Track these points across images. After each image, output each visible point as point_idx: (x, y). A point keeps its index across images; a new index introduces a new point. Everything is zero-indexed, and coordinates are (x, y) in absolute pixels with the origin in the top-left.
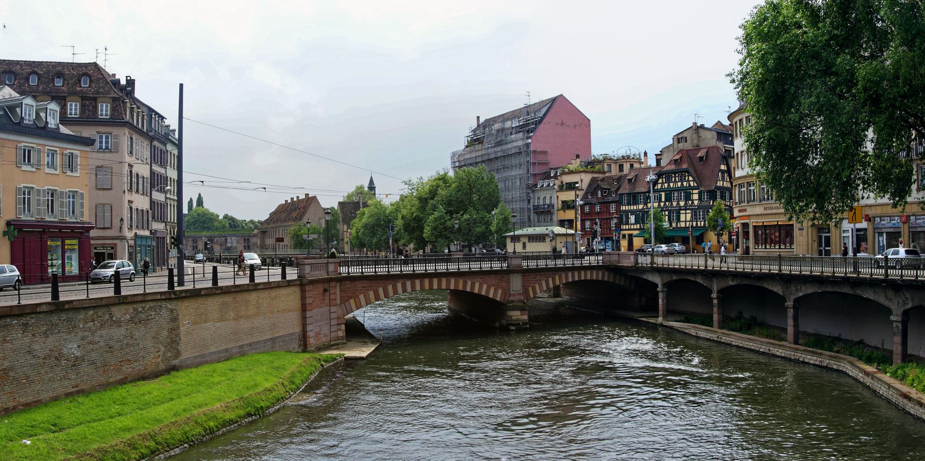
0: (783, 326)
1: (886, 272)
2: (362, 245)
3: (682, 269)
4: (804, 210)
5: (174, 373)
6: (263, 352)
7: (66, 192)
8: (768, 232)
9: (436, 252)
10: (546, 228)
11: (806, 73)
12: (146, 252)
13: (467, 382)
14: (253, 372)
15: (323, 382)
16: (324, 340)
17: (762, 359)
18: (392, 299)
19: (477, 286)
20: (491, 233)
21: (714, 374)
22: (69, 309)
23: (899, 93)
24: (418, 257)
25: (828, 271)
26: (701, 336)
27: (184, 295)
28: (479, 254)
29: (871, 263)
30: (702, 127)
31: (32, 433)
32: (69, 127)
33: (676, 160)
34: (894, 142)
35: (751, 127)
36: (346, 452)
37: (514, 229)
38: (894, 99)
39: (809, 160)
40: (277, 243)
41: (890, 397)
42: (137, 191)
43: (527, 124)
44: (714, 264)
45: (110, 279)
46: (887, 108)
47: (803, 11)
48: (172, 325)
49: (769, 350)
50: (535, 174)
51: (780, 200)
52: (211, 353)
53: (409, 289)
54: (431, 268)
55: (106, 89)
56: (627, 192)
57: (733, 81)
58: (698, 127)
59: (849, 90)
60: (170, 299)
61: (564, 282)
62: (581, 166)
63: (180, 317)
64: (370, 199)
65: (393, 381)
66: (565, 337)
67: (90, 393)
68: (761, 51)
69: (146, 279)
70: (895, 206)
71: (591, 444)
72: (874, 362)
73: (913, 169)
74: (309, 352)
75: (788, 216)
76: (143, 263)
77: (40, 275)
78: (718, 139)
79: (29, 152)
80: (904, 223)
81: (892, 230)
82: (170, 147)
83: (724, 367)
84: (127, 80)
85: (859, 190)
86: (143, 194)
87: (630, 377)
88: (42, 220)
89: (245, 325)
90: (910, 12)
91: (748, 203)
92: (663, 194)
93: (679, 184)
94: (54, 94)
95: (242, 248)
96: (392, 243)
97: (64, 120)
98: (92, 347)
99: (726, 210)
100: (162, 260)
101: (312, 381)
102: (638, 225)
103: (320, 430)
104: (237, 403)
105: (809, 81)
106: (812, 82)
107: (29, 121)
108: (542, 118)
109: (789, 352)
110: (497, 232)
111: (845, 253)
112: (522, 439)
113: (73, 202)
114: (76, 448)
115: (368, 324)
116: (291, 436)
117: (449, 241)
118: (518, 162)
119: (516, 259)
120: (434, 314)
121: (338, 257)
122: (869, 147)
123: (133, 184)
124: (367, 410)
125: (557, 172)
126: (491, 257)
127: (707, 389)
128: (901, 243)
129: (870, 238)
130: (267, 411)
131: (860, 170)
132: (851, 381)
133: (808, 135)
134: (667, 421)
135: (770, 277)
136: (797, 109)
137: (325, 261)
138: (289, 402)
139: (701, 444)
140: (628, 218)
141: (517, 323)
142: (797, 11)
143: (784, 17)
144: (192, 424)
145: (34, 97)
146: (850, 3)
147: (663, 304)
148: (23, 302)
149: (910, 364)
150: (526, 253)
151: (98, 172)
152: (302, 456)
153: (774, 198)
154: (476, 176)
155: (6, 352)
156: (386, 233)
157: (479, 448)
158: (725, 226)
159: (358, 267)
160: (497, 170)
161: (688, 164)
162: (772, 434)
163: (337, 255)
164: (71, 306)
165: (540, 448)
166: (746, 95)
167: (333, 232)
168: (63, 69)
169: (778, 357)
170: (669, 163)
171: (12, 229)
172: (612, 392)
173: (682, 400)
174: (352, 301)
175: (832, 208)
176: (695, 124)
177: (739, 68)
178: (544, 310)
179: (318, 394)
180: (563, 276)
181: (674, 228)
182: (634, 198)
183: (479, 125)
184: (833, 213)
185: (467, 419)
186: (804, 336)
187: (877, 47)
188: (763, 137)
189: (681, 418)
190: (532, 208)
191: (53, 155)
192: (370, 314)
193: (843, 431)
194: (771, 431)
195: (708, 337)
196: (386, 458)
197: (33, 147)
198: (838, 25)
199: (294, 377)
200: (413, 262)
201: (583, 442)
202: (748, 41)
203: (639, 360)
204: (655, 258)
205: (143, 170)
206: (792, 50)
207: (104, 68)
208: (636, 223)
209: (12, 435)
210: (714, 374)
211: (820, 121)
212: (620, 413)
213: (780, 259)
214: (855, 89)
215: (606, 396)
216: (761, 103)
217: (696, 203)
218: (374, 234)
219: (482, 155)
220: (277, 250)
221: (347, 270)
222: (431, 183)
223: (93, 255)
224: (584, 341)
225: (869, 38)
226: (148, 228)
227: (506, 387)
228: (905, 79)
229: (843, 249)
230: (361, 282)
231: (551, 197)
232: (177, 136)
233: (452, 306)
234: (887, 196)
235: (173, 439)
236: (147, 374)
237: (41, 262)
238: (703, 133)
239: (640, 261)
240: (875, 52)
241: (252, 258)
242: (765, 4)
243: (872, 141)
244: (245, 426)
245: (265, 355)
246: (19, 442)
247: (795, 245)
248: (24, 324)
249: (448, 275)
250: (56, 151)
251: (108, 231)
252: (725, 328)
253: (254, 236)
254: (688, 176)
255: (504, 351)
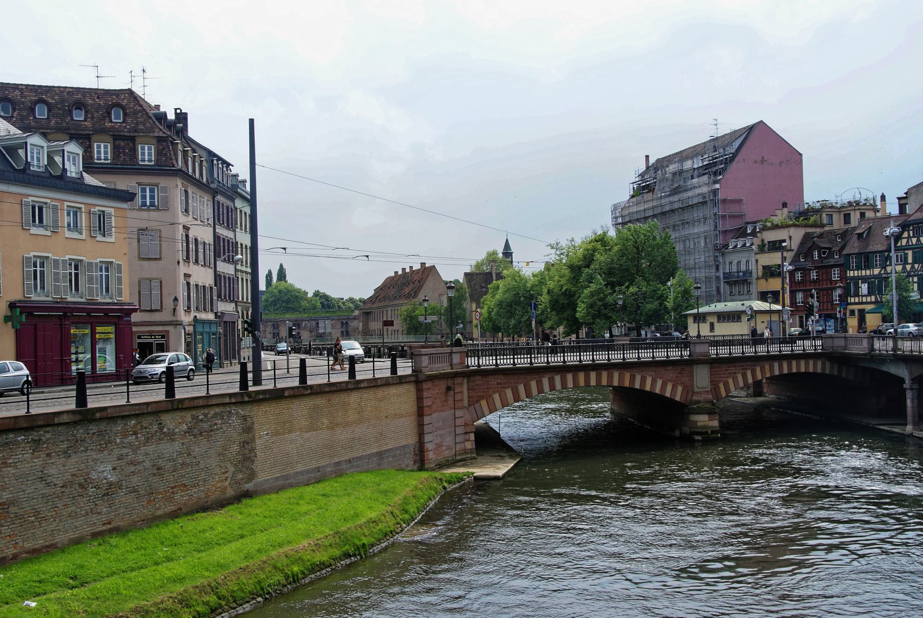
2: (496, 329)
5: (246, 501)
7: (96, 264)
9: (593, 337)
10: (742, 302)
12: (210, 342)
13: (638, 511)
14: (353, 497)
15: (446, 510)
16: (447, 454)
18: (536, 399)
19: (649, 381)
20: (667, 310)
22: (101, 419)
24: (570, 343)
27: (261, 397)
28: (651, 339)
31: (40, 591)
32: (97, 176)
36: (476, 606)
37: (698, 305)
40: (385, 328)
42: (197, 262)
43: (714, 163)
45: (160, 378)
48: (245, 437)
52: (297, 472)
53: (558, 386)
54: (587, 358)
55: (148, 125)
56: (856, 251)
60: (243, 403)
63: (256, 426)
64: (505, 268)
65: (538, 509)
66: (771, 451)
67: (128, 531)
69: (209, 376)
71: (813, 602)
74: (427, 470)
76: (205, 355)
77: (60, 373)
79: (41, 209)
82: (239, 203)
84: (176, 113)
86: (204, 265)
88: (63, 301)
89: (342, 435)
92: (910, 253)
94: (73, 132)
95: (339, 335)
96: (536, 326)
97: (90, 166)
98: (132, 468)
100: (232, 352)
101: (430, 509)
102: (873, 297)
103: (441, 576)
104: (331, 540)
107: (39, 167)
108: (735, 155)
110: (675, 310)
112: (715, 591)
113: (107, 276)
114: (103, 609)
115: (505, 433)
116: (402, 584)
117: (611, 322)
118: (701, 215)
119: (701, 345)
120: (593, 419)
121: (465, 345)
123: (191, 253)
124: (503, 548)
125: (755, 227)
126: (667, 342)
130: (371, 551)
137: (448, 350)
138: (400, 538)
140: (857, 287)
141: (704, 431)
144: (269, 569)
145: (44, 135)
147: (913, 407)
148: (33, 411)
150: (714, 336)
151: (141, 237)
152: (416, 611)
154: (645, 236)
155: (6, 479)
156: (527, 312)
157: (655, 602)
159: (491, 358)
163: (464, 342)
164: (104, 414)
165: (741, 605)
167: (458, 312)
168: (84, 96)
171: (18, 313)
172: (841, 528)
174: (484, 403)
178: (741, 414)
179: (438, 526)
180: (767, 367)
182: (866, 260)
183: (648, 168)
185: (639, 561)
190: (722, 276)
191: (75, 214)
192: (507, 419)
196: (530, 614)
197: (46, 203)
199: (407, 504)
200: (563, 350)
201: (801, 599)
204: (900, 343)
205: (205, 234)
207: (143, 97)
209: (8, 595)
212: (854, 560)
215: (832, 535)
219: (653, 207)
220: (385, 336)
221: (476, 362)
223: (136, 346)
224: (799, 457)
226: (212, 310)
227: (690, 519)
230: (496, 377)
231: (747, 262)
232: (248, 188)
233: (616, 408)
235: (242, 591)
236: (209, 503)
237: (62, 357)
241: (353, 348)
244: (341, 571)
245: (369, 474)
246: (19, 605)
248: (35, 441)
249: (609, 367)
250: (80, 208)
251: (157, 314)
253: (355, 318)
255: (687, 468)
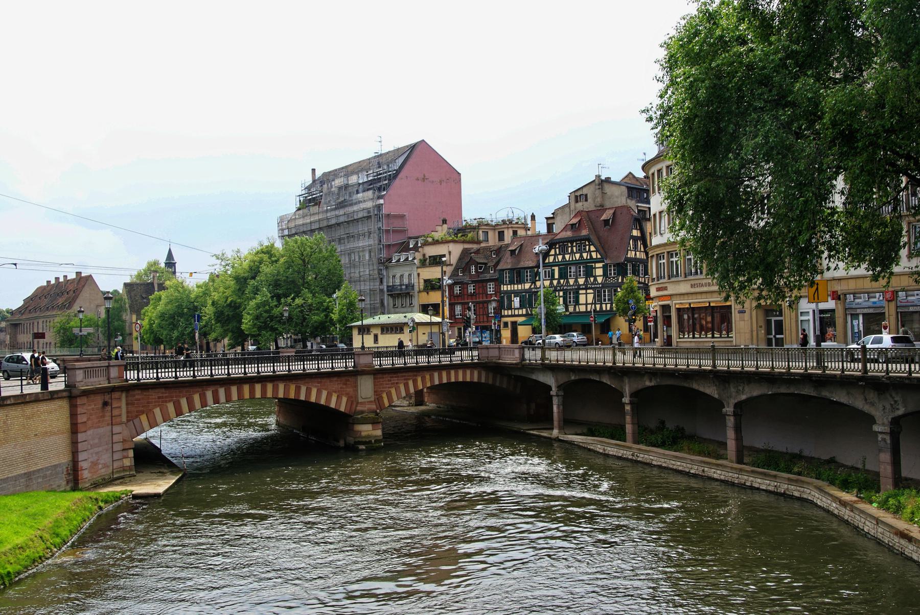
0: (721, 439)
1: (865, 367)
2: (158, 341)
3: (583, 366)
4: (745, 287)
6: (13, 494)
8: (696, 316)
10: (404, 315)
11: (750, 105)
16: (104, 472)
17: (694, 483)
20: (332, 323)
21: (630, 504)
23: (883, 127)
25: (780, 366)
26: (611, 453)
29: (842, 355)
30: (608, 180)
33: (573, 225)
34: (874, 193)
35: (674, 180)
38: (877, 135)
39: (752, 220)
40: (36, 340)
41: (880, 536)
43: (378, 179)
44: (625, 359)
46: (865, 148)
47: (749, 20)
49: (703, 471)
50: (389, 245)
51: (713, 274)
56: (509, 267)
57: (650, 119)
58: (602, 181)
59: (811, 126)
61: (429, 385)
62: (448, 233)
68: (689, 77)
70: (875, 278)
72: (853, 488)
73: (902, 229)
74: (81, 490)
75: (724, 295)
78: (629, 196)
80: (889, 301)
81: (871, 311)
83: (642, 494)
85: (823, 258)
87: (518, 510)
90: (906, 12)
91: (669, 279)
92: (556, 269)
93: (578, 256)
96: (199, 338)
99: (639, 288)
102: (524, 310)
105: (754, 115)
106: (759, 116)
108: (398, 172)
109: (731, 474)
110: (340, 321)
111: (805, 341)
115: (166, 449)
117: (276, 334)
118: (366, 229)
122: (838, 201)
125: (417, 242)
126: (332, 354)
127: (622, 523)
128: (885, 328)
129: (839, 321)
131: (824, 232)
132: (821, 513)
133: (751, 188)
134: (569, 567)
135: (700, 374)
136: (736, 153)
139: (617, 599)
140: (510, 301)
142: (741, 20)
143: (723, 30)
146: (817, 6)
147: (559, 412)
149: (907, 491)
153: (704, 272)
156: (191, 324)
158: (638, 309)
159: (151, 371)
160: (340, 239)
161: (590, 229)
162: (714, 585)
166: (667, 137)
167: (116, 323)
169: (717, 480)
170: (564, 229)
173: (589, 539)
174: (144, 418)
175: (785, 283)
176: (598, 176)
177: (658, 101)
180: (428, 377)
181: (571, 313)
182: (518, 275)
183: (314, 181)
184: (786, 290)
186: (751, 453)
187: (853, 65)
188: (690, 192)
189: (588, 563)
190: (385, 289)
193: (814, 582)
194: (711, 581)
195: (620, 455)
198: (798, 37)
202: (671, 64)
203: (529, 486)
204: (547, 353)
206: (731, 75)
208: (521, 307)
210: (630, 504)
211: (769, 169)
213: (714, 351)
214: (819, 124)
216: (687, 147)
217: (600, 280)
218: (174, 326)
219: (319, 220)
222: (250, 257)
225: (842, 53)
228: (894, 108)
229: (802, 336)
230: (157, 391)
231: (410, 275)
234: (864, 266)
238: (608, 189)
239: (527, 356)
240: (851, 71)
242: (696, 13)
243: (842, 193)
245: (16, 498)
247: (734, 332)
249: (275, 378)
252: (642, 443)
254: (589, 245)
